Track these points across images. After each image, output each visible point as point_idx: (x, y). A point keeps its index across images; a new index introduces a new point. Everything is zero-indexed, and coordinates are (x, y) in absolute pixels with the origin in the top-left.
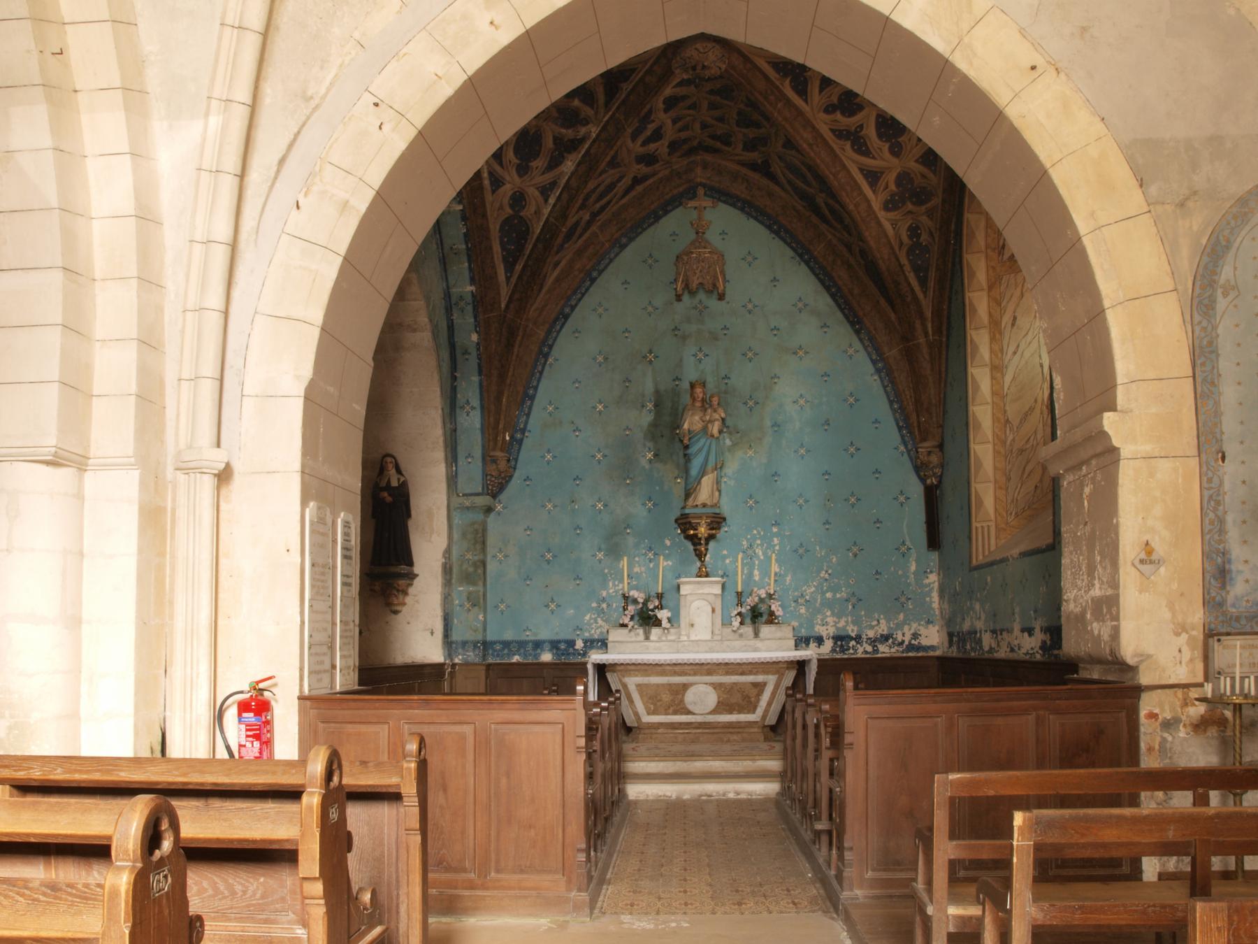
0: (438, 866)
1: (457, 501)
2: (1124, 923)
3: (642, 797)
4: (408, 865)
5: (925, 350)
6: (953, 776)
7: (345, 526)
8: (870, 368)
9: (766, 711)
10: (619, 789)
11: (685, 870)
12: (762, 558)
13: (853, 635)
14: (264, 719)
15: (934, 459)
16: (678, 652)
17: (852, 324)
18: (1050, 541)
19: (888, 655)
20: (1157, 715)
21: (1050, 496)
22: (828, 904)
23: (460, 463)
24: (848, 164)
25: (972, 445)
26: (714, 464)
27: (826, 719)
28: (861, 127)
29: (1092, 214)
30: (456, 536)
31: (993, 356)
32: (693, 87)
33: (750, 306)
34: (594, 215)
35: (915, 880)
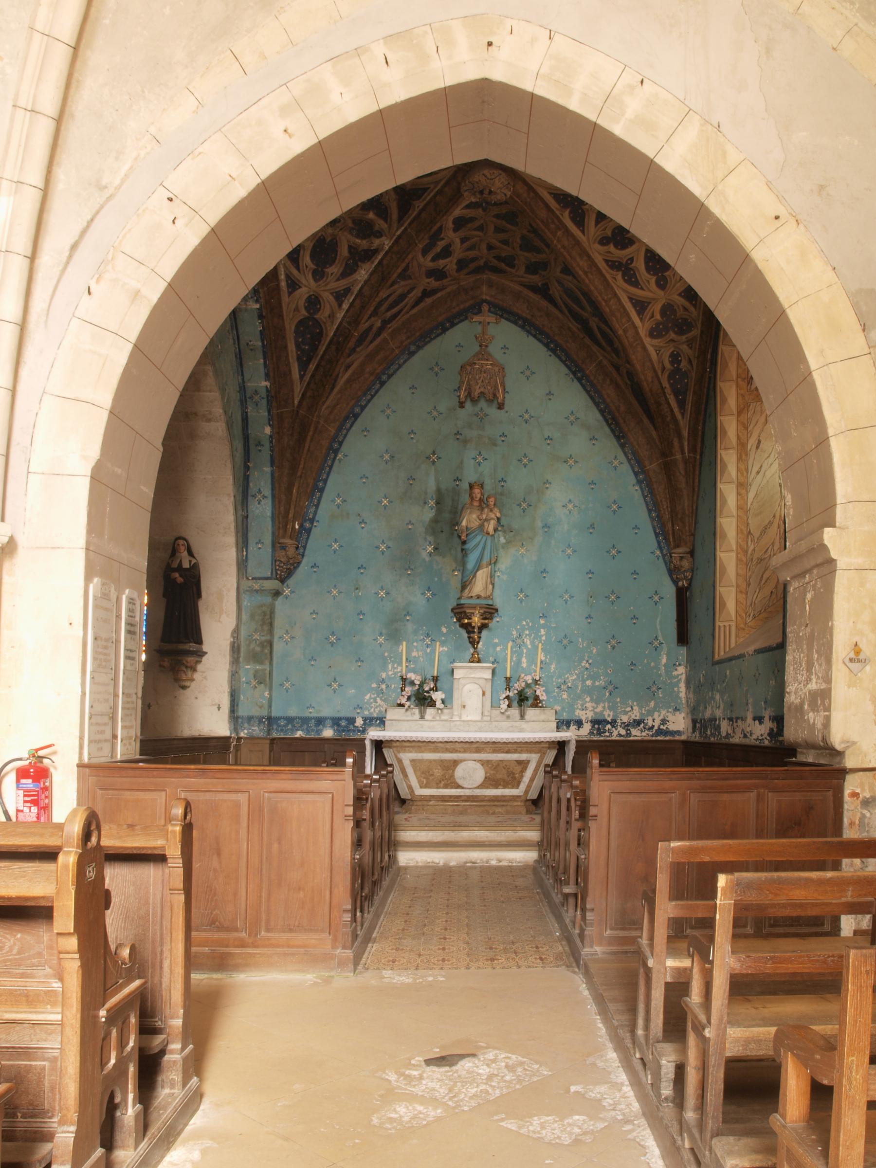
0: (210, 926)
1: (246, 584)
2: (807, 971)
3: (412, 864)
4: (171, 922)
5: (681, 466)
6: (674, 844)
7: (130, 603)
8: (632, 479)
9: (529, 787)
10: (389, 856)
11: (446, 929)
12: (530, 647)
13: (609, 719)
14: (42, 785)
15: (686, 564)
16: (450, 731)
17: (618, 438)
18: (780, 640)
19: (639, 738)
20: (858, 794)
21: (781, 602)
22: (572, 959)
23: (250, 548)
24: (619, 292)
25: (718, 553)
26: (488, 560)
27: (576, 794)
28: (632, 259)
29: (822, 352)
30: (245, 617)
31: (739, 474)
32: (480, 210)
33: (526, 416)
34: (385, 323)
35: (641, 937)
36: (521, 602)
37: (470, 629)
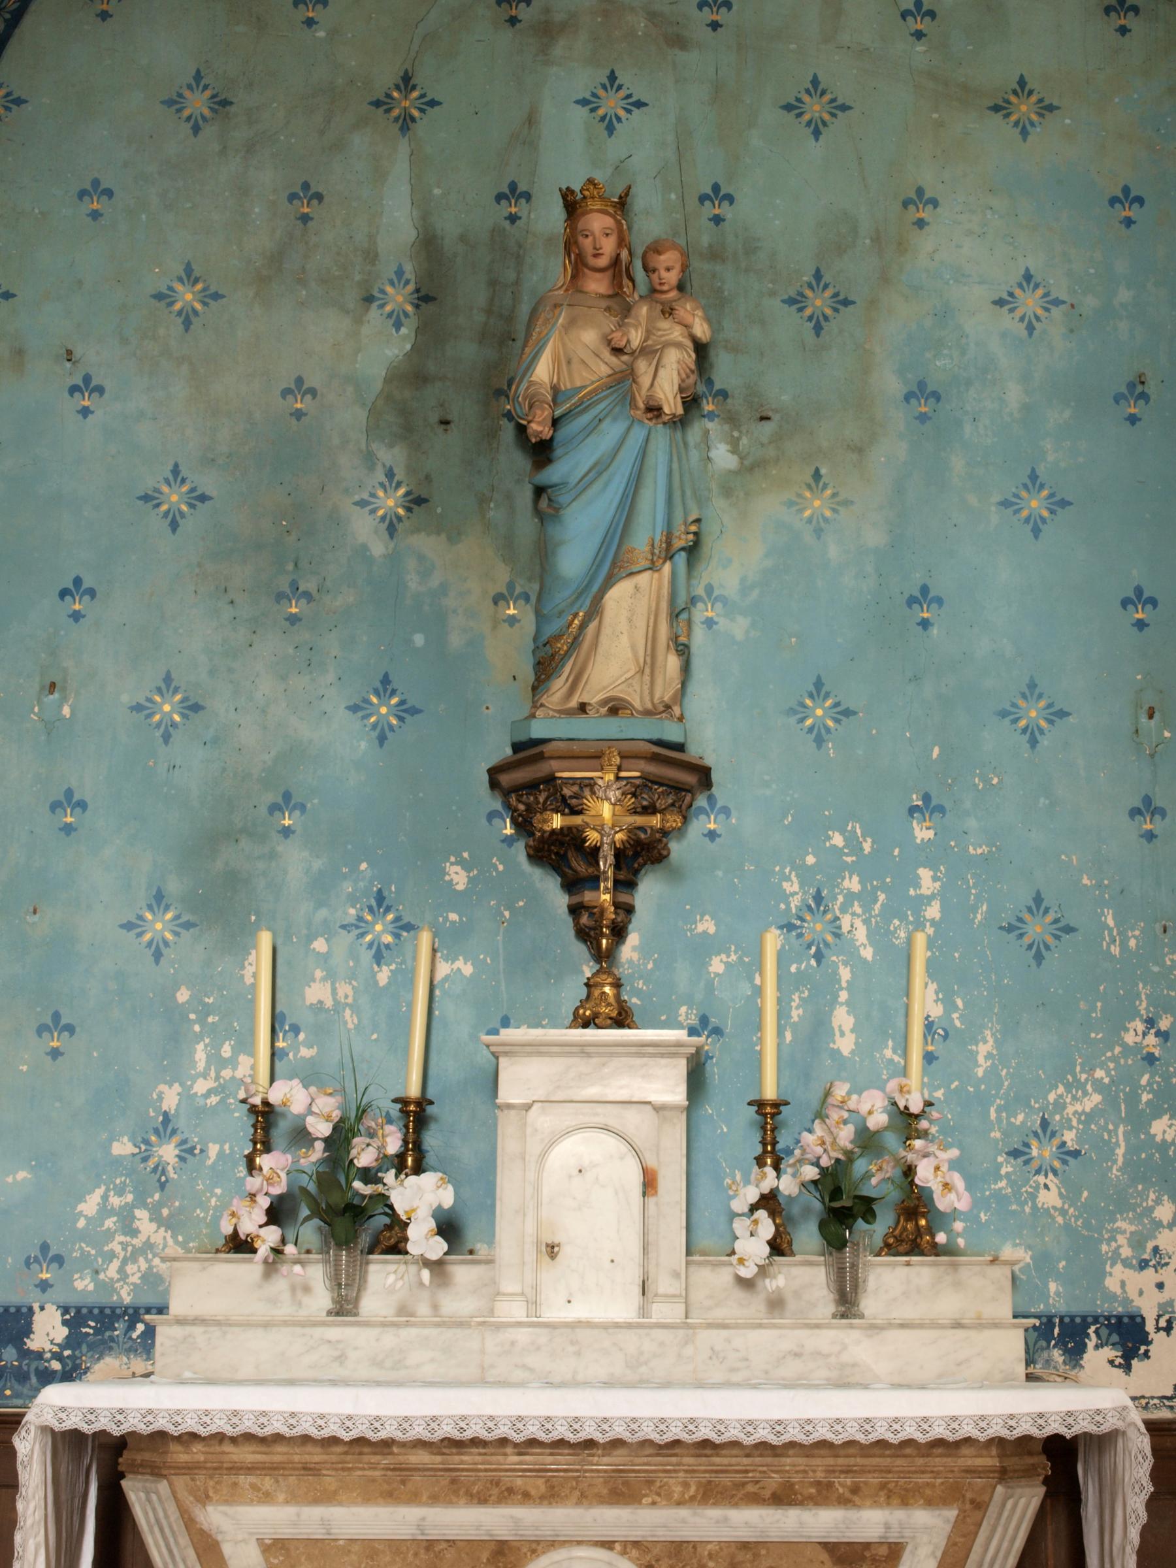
12: (867, 953)
36: (819, 741)
37: (581, 867)
